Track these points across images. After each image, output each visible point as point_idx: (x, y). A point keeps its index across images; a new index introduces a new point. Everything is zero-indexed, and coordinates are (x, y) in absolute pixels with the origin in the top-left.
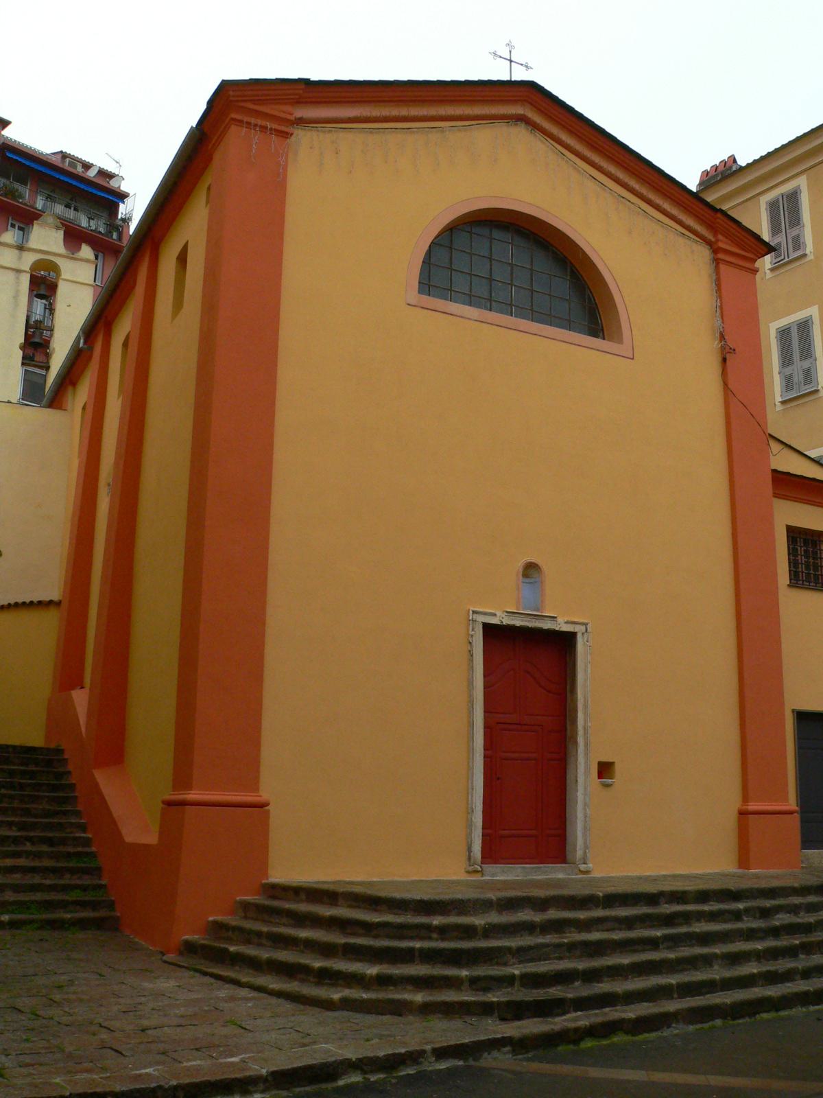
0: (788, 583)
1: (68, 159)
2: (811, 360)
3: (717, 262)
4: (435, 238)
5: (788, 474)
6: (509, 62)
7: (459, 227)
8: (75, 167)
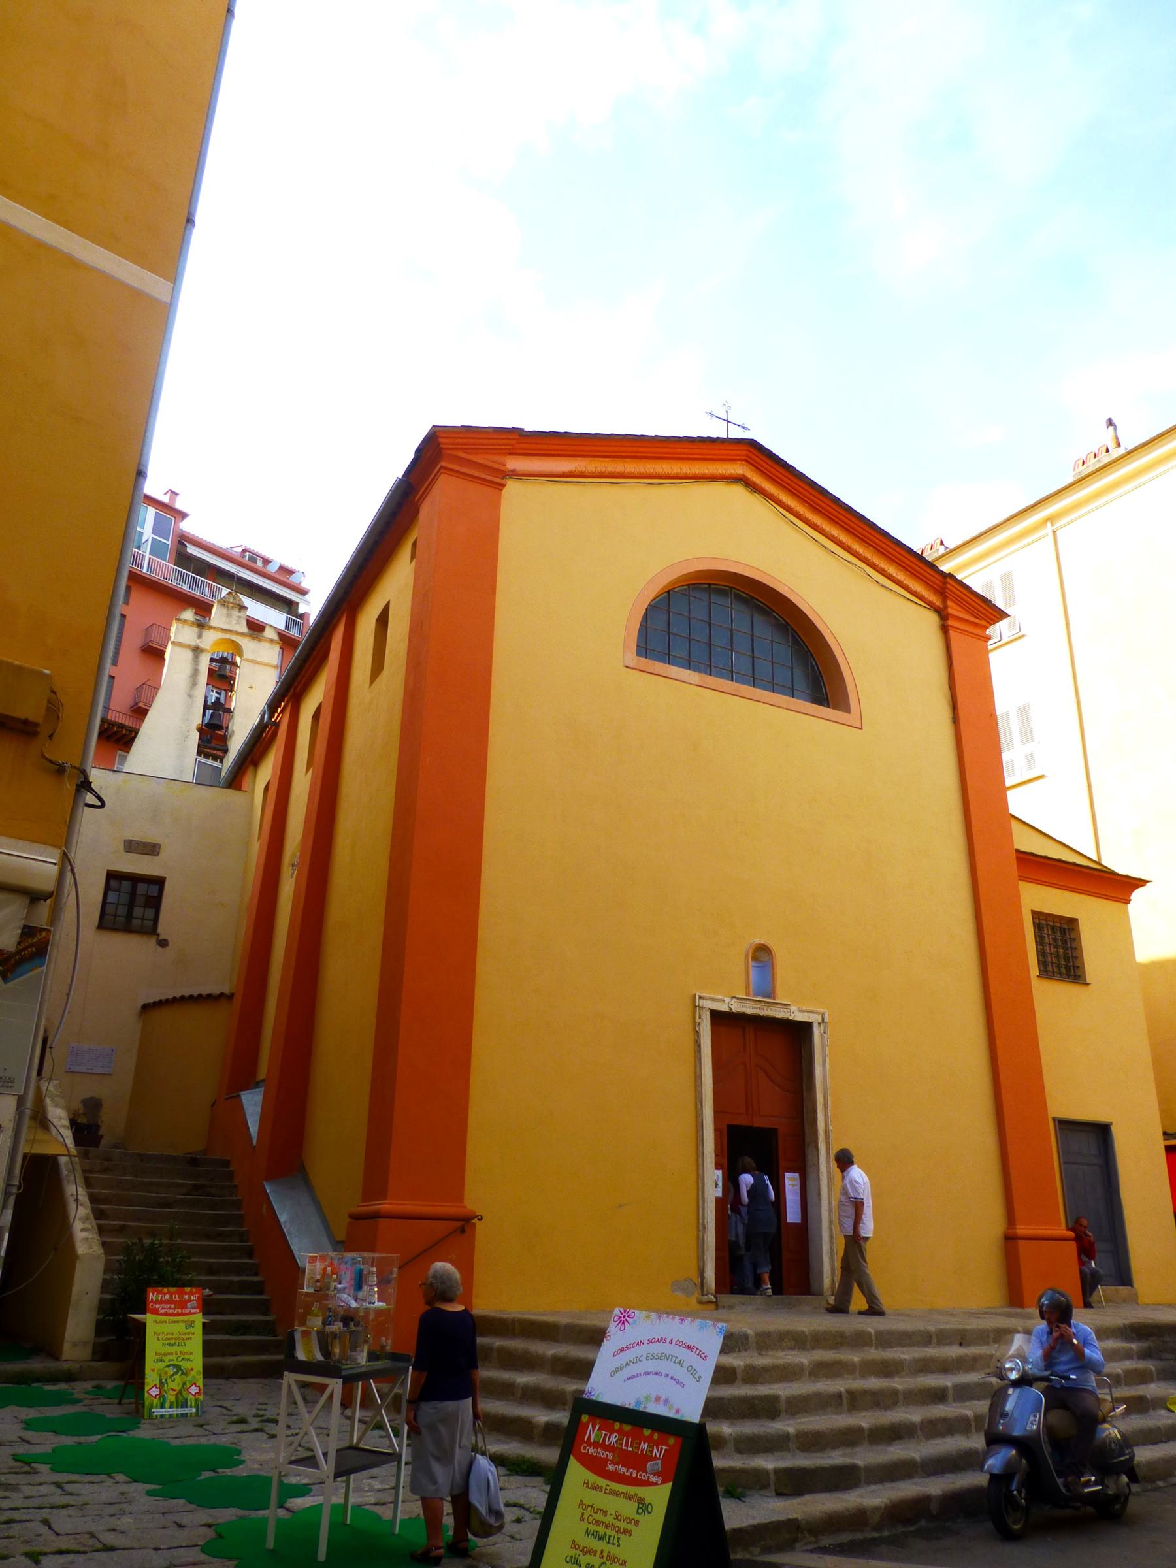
0: (1038, 974)
1: (247, 553)
3: (945, 629)
4: (651, 602)
5: (1032, 854)
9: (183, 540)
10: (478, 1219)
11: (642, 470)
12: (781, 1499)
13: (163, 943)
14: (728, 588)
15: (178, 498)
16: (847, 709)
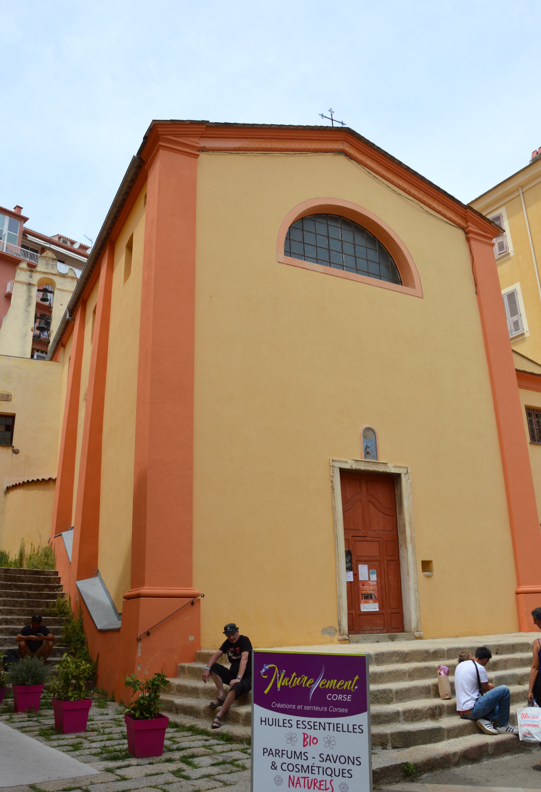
1: (62, 239)
2: (518, 315)
3: (468, 240)
6: (331, 120)
7: (307, 217)
8: (66, 243)
9: (26, 233)
10: (202, 596)
11: (282, 146)
12: (396, 750)
13: (16, 452)
14: (338, 217)
15: (22, 210)
16: (414, 287)
